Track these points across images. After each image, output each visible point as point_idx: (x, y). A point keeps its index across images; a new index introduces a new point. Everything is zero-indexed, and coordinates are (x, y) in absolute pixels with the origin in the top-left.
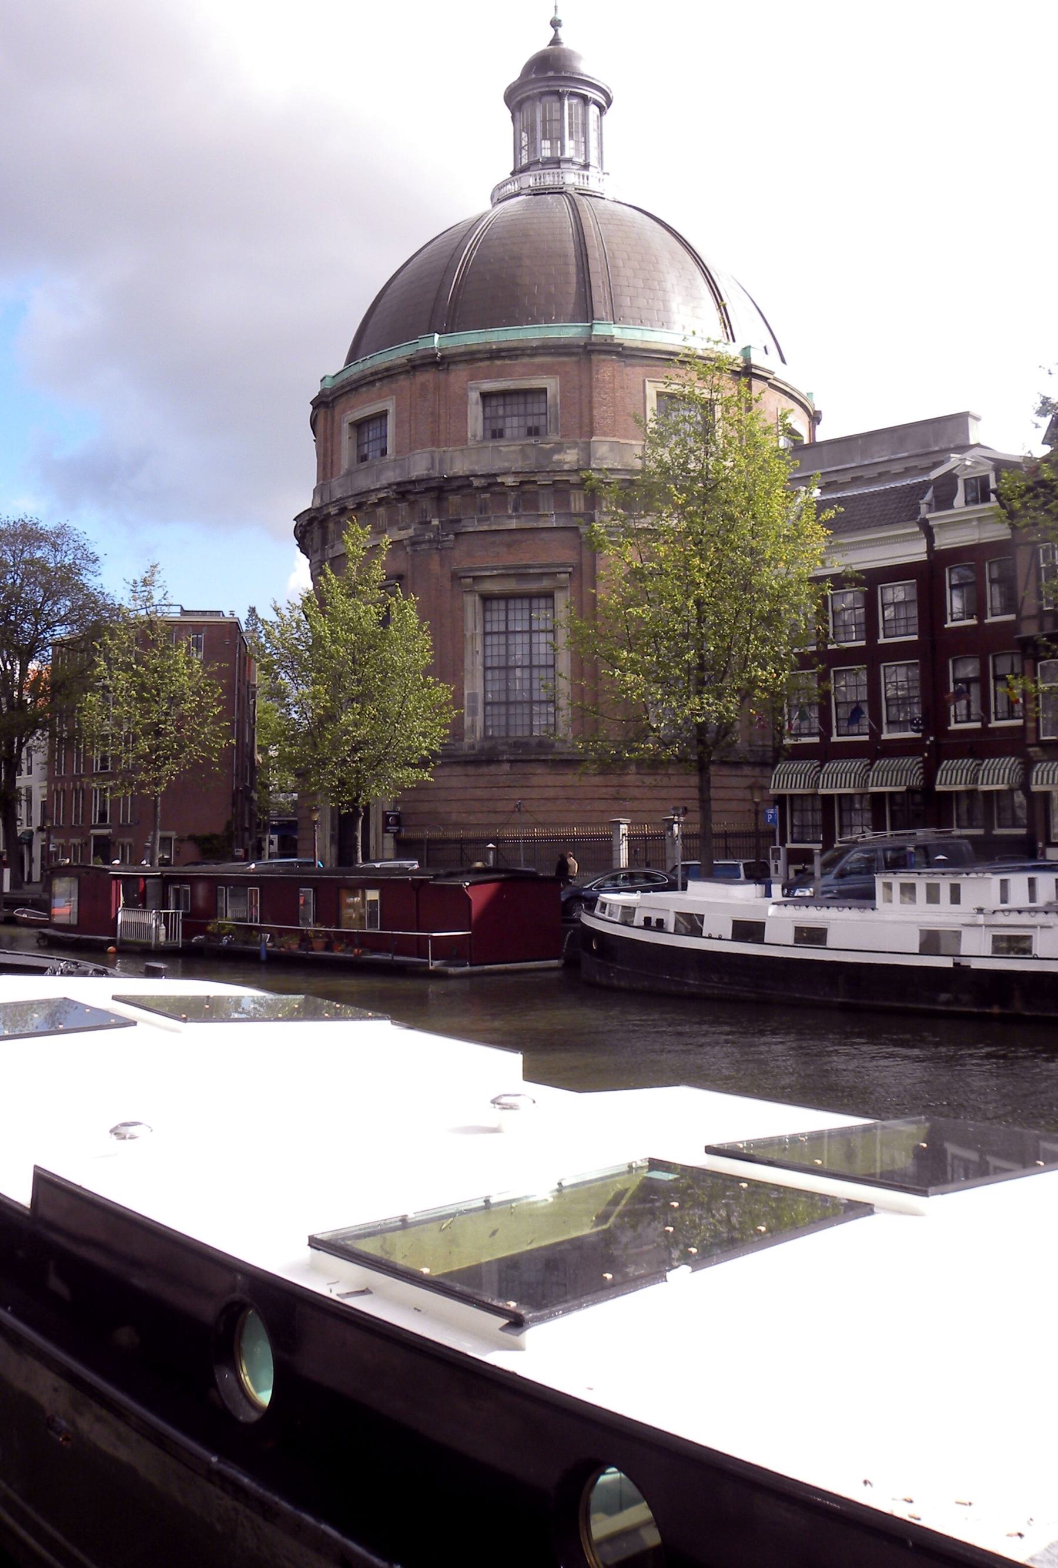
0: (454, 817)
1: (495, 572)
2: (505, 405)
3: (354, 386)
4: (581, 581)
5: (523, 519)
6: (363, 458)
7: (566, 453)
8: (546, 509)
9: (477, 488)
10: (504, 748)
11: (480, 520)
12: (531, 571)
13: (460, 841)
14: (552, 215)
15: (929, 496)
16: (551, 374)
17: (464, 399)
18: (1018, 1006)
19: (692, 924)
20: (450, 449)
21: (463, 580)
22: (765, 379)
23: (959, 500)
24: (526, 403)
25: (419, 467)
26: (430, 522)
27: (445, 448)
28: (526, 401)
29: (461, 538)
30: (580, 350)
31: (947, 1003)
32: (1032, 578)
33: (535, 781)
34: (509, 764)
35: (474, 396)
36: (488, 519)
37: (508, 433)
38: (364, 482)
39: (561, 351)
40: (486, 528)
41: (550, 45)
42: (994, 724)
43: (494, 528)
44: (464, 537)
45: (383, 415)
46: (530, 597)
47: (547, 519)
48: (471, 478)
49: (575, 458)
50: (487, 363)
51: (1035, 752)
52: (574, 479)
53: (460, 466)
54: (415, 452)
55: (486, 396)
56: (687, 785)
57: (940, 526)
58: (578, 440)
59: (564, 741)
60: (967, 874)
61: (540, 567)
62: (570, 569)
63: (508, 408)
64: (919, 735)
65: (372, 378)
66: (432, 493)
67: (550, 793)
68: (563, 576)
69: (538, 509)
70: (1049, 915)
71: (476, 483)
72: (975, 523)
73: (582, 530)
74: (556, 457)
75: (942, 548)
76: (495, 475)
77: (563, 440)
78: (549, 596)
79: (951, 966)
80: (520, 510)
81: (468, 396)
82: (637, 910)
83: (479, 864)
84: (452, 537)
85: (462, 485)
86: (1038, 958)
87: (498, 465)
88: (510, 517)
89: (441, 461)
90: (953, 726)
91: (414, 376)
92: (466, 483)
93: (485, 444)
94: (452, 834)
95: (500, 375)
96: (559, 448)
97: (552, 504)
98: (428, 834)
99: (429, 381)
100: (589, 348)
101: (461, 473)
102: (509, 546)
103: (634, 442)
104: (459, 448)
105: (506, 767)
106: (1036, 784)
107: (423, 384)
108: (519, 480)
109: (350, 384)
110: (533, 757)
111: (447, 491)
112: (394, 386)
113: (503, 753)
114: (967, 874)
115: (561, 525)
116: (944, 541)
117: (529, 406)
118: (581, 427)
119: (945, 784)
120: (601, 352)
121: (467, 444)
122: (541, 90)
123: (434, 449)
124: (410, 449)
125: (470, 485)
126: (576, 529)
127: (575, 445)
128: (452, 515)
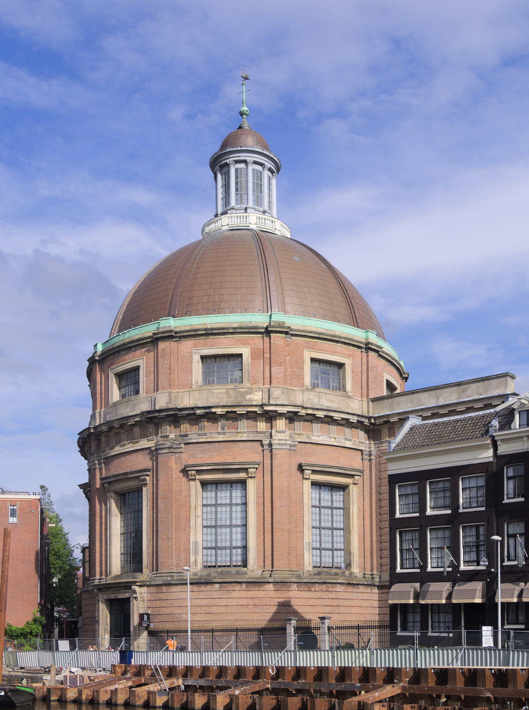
1: (209, 468)
10: (216, 574)
22: (377, 352)
27: (178, 390)
33: (234, 594)
35: (196, 358)
38: (126, 411)
39: (252, 330)
43: (209, 440)
45: (137, 369)
55: (204, 358)
57: (502, 440)
62: (257, 466)
67: (244, 602)
72: (525, 439)
73: (264, 442)
74: (248, 397)
78: (243, 483)
80: (225, 429)
88: (219, 433)
92: (192, 412)
95: (212, 346)
96: (250, 391)
101: (188, 406)
105: (217, 586)
113: (215, 578)
116: (504, 449)
126: (261, 441)
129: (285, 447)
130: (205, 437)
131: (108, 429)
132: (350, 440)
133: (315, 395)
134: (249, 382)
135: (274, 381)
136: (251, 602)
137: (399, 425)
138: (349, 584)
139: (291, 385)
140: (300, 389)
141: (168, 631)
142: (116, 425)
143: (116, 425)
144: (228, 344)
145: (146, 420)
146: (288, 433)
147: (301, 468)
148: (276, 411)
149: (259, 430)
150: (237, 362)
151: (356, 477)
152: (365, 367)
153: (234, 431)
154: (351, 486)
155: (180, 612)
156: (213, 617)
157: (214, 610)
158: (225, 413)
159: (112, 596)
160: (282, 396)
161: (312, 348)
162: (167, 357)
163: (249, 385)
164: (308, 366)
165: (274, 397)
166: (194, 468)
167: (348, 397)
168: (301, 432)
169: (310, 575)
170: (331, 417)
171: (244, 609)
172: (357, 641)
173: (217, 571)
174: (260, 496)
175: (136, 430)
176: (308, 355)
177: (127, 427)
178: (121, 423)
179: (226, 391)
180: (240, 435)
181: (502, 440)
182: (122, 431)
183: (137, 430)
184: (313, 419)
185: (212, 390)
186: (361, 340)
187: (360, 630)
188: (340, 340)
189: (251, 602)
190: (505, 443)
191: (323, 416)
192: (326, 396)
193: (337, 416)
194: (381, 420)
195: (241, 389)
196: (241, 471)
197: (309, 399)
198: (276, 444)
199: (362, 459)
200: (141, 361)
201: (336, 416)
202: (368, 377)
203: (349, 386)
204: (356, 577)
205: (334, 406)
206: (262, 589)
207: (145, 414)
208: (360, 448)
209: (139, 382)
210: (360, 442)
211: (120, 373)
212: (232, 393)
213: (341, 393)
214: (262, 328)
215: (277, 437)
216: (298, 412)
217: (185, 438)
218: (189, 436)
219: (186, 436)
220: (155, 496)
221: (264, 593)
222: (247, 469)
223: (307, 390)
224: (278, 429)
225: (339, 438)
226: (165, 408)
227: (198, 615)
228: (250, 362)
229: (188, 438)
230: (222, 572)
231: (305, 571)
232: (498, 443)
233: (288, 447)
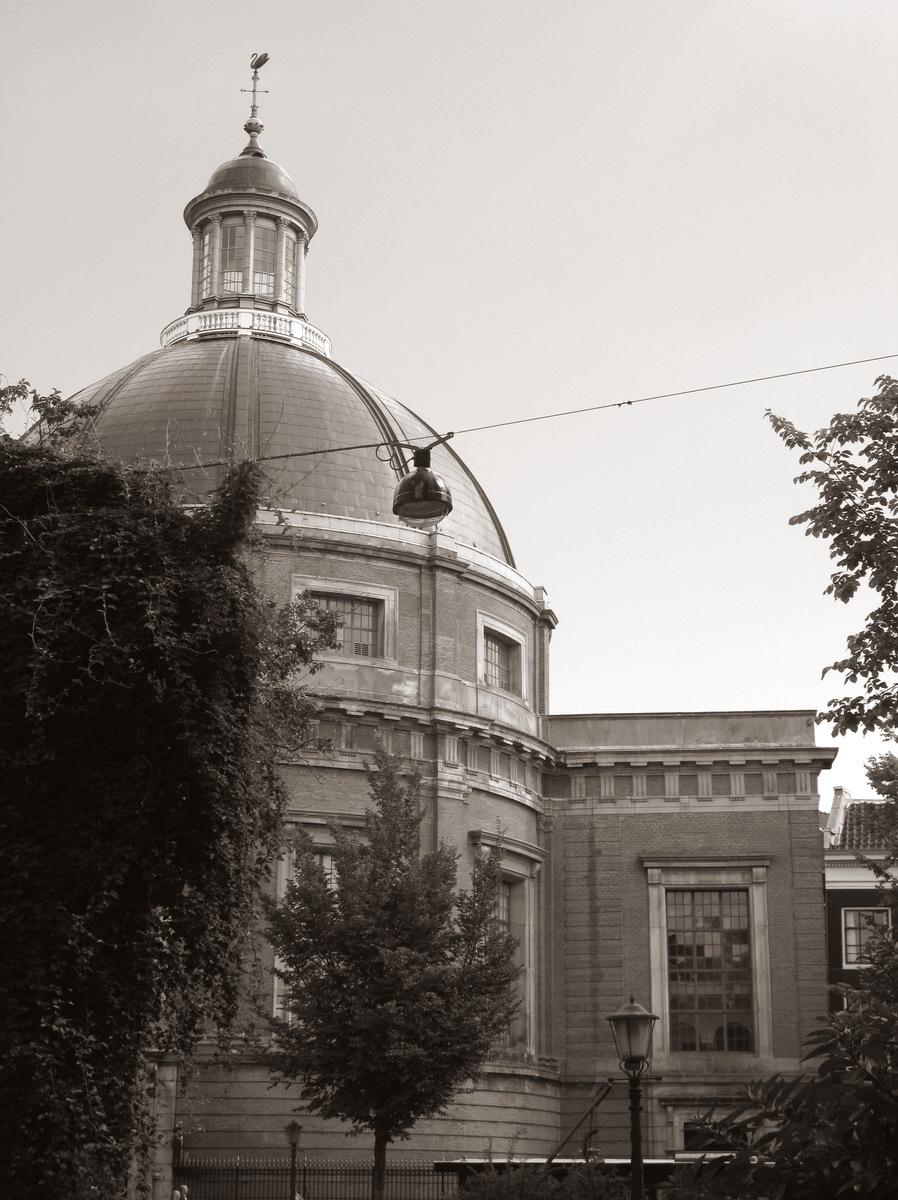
2: (352, 612)
14: (284, 365)
28: (353, 610)
39: (405, 559)
41: (242, 154)
50: (318, 555)
56: (513, 1105)
62: (767, 863)
74: (396, 687)
88: (343, 753)
95: (331, 574)
96: (398, 678)
103: (467, 683)
108: (364, 709)
120: (445, 569)
122: (260, 210)
134: (395, 658)
135: (440, 663)
137: (609, 774)
154: (526, 883)
164: (481, 641)
166: (295, 819)
172: (446, 1186)
179: (357, 671)
185: (333, 665)
194: (579, 761)
211: (605, 748)
212: (367, 674)
215: (447, 775)
220: (543, 989)
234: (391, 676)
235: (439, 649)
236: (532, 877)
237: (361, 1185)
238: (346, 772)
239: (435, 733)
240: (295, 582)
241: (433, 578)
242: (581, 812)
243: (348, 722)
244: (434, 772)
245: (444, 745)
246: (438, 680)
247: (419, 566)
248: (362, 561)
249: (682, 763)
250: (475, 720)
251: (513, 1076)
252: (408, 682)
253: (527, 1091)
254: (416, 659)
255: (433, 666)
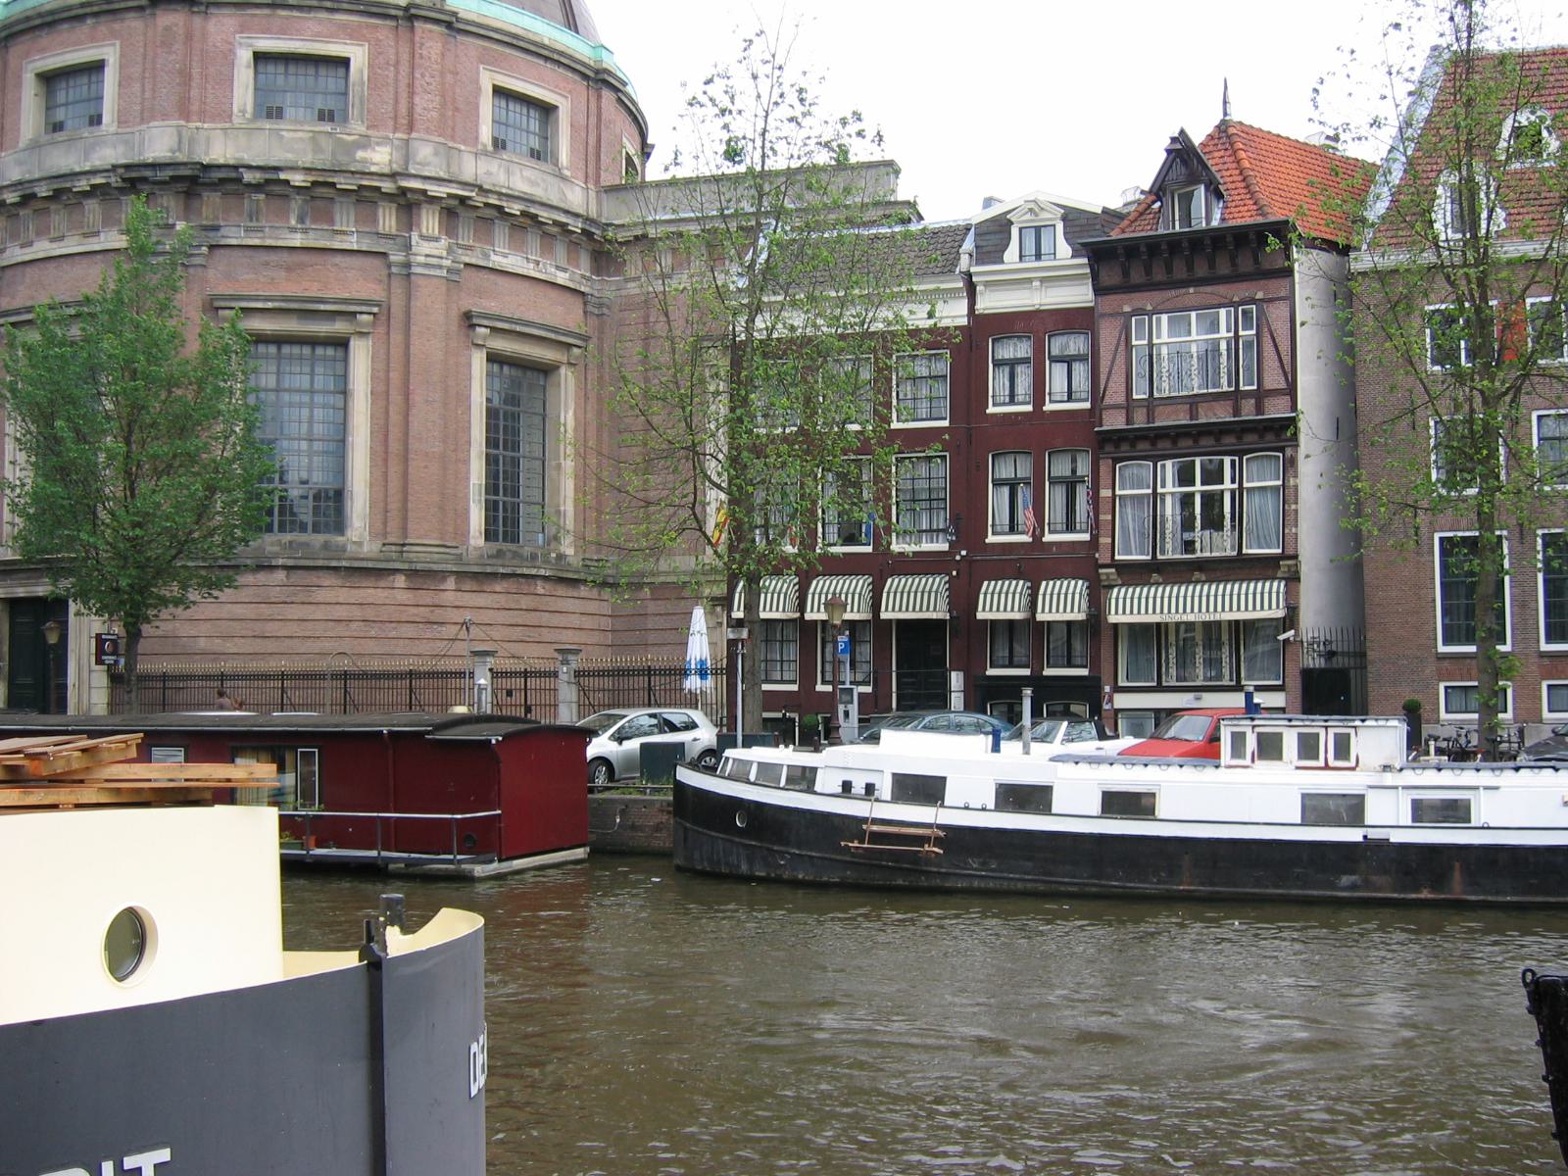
0: (202, 643)
1: (270, 305)
2: (286, 74)
3: (49, 19)
4: (389, 326)
5: (311, 234)
6: (58, 127)
7: (374, 150)
8: (344, 224)
9: (249, 185)
10: (276, 549)
11: (247, 230)
12: (322, 307)
13: (164, 677)
15: (968, 245)
16: (357, 39)
17: (230, 62)
18: (1457, 889)
19: (924, 789)
20: (206, 126)
21: (220, 312)
22: (616, 90)
23: (1011, 254)
24: (317, 76)
25: (159, 144)
26: (174, 225)
27: (199, 124)
28: (317, 72)
29: (218, 252)
30: (400, 13)
31: (1353, 887)
32: (1121, 359)
33: (321, 595)
34: (285, 572)
35: (245, 56)
36: (260, 230)
37: (289, 112)
38: (62, 160)
40: (257, 242)
42: (1048, 538)
43: (269, 242)
44: (222, 251)
45: (97, 67)
46: (313, 342)
47: (345, 237)
48: (241, 170)
49: (387, 158)
50: (266, 11)
51: (1107, 574)
52: (387, 186)
53: (219, 150)
54: (151, 124)
55: (260, 57)
57: (987, 284)
58: (391, 135)
59: (360, 544)
60: (1363, 721)
61: (335, 303)
62: (375, 310)
63: (292, 79)
64: (945, 547)
65: (81, 11)
66: (179, 185)
67: (341, 612)
68: (365, 317)
69: (332, 222)
70: (1481, 773)
71: (248, 177)
72: (1036, 284)
73: (392, 258)
74: (360, 154)
75: (986, 312)
76: (277, 169)
77: (370, 132)
78: (342, 343)
79: (1361, 839)
80: (308, 222)
81: (235, 54)
82: (820, 773)
83: (461, 710)
84: (204, 249)
85: (227, 181)
86: (1489, 828)
87: (277, 156)
88: (293, 230)
89: (192, 141)
90: (991, 539)
91: (153, 15)
92: (233, 175)
93: (258, 125)
94: (199, 666)
95: (283, 32)
96: (365, 143)
97: (352, 218)
98: (167, 666)
99: (177, 25)
100: (413, 11)
101: (222, 161)
102: (289, 269)
103: (463, 148)
104: (219, 126)
105: (281, 575)
106: (1117, 613)
107: (167, 29)
108: (311, 179)
109: (40, 15)
110: (320, 563)
111: (204, 184)
112: (117, 26)
113: (276, 556)
114: (1363, 721)
115: (364, 249)
116: (990, 302)
117: (322, 80)
118: (396, 118)
119: (921, 610)
120: (427, 19)
121: (231, 121)
123: (183, 123)
124: (142, 119)
125: (239, 180)
126: (384, 254)
127: (386, 141)
128: (207, 219)
129: (438, 272)
130: (260, 235)
131: (18, 199)
132: (565, 270)
133: (500, 167)
134: (362, 122)
135: (418, 125)
136: (357, 613)
138: (561, 580)
139: (453, 138)
140: (469, 149)
141: (222, 675)
142: (43, 191)
143: (43, 191)
144: (318, 34)
145: (120, 185)
146: (444, 242)
147: (469, 320)
148: (424, 192)
149: (381, 230)
150: (341, 71)
151: (576, 351)
152: (593, 120)
153: (326, 227)
154: (563, 370)
155: (193, 633)
156: (271, 646)
157: (271, 628)
158: (309, 185)
159: (21, 592)
160: (435, 160)
161: (494, 62)
162: (176, 46)
163: (362, 129)
164: (486, 104)
165: (418, 160)
167: (564, 178)
168: (471, 242)
169: (482, 556)
170: (534, 217)
171: (340, 630)
173: (280, 541)
174: (378, 378)
175: (91, 207)
176: (487, 80)
177: (69, 199)
178: (55, 186)
180: (339, 237)
181: (987, 284)
182: (53, 207)
183: (92, 205)
184: (497, 218)
186: (587, 61)
187: (652, 678)
188: (551, 55)
189: (357, 613)
190: (991, 291)
191: (518, 213)
192: (521, 170)
193: (545, 214)
195: (345, 137)
196: (338, 318)
197: (489, 173)
198: (419, 265)
199: (585, 312)
200: (110, 50)
201: (544, 215)
202: (599, 141)
203: (564, 156)
204: (569, 564)
205: (538, 192)
206: (382, 584)
207: (121, 171)
208: (583, 289)
209: (102, 98)
210: (583, 277)
212: (324, 141)
213: (547, 167)
214: (397, 7)
215: (422, 250)
216: (469, 198)
217: (212, 234)
218: (222, 230)
219: (216, 228)
221: (386, 593)
222: (354, 314)
223: (485, 153)
224: (424, 231)
225: (544, 264)
226: (168, 161)
227: (236, 639)
228: (366, 78)
229: (219, 234)
230: (291, 542)
231: (470, 549)
232: (978, 288)
233: (444, 273)
234: (353, 142)
235: (418, 109)
236: (570, 364)
237: (636, 687)
238: (299, 251)
239: (408, 203)
240: (240, 44)
241: (412, 28)
242: (637, 291)
243: (298, 194)
244: (408, 247)
245: (419, 216)
246: (414, 144)
247: (395, 18)
248: (324, 15)
249: (172, 177)
250: (454, 185)
251: (514, 575)
252: (377, 148)
253: (542, 591)
254: (391, 123)
255: (411, 127)
